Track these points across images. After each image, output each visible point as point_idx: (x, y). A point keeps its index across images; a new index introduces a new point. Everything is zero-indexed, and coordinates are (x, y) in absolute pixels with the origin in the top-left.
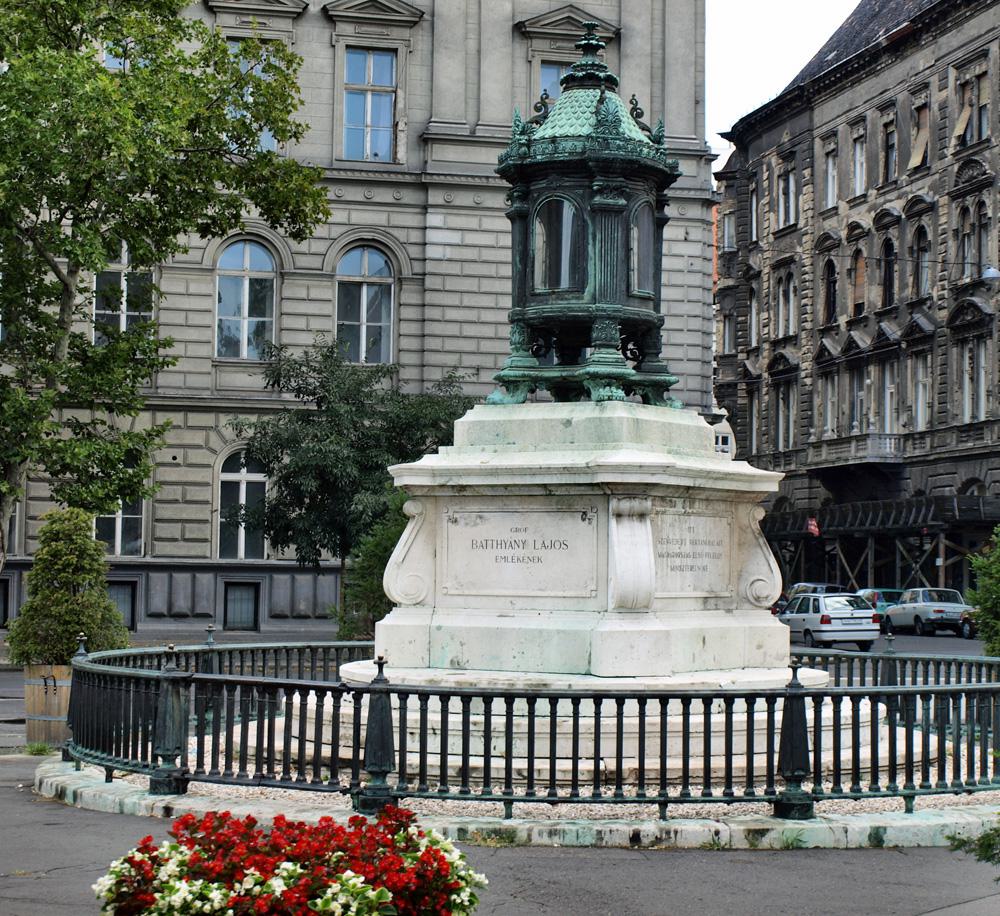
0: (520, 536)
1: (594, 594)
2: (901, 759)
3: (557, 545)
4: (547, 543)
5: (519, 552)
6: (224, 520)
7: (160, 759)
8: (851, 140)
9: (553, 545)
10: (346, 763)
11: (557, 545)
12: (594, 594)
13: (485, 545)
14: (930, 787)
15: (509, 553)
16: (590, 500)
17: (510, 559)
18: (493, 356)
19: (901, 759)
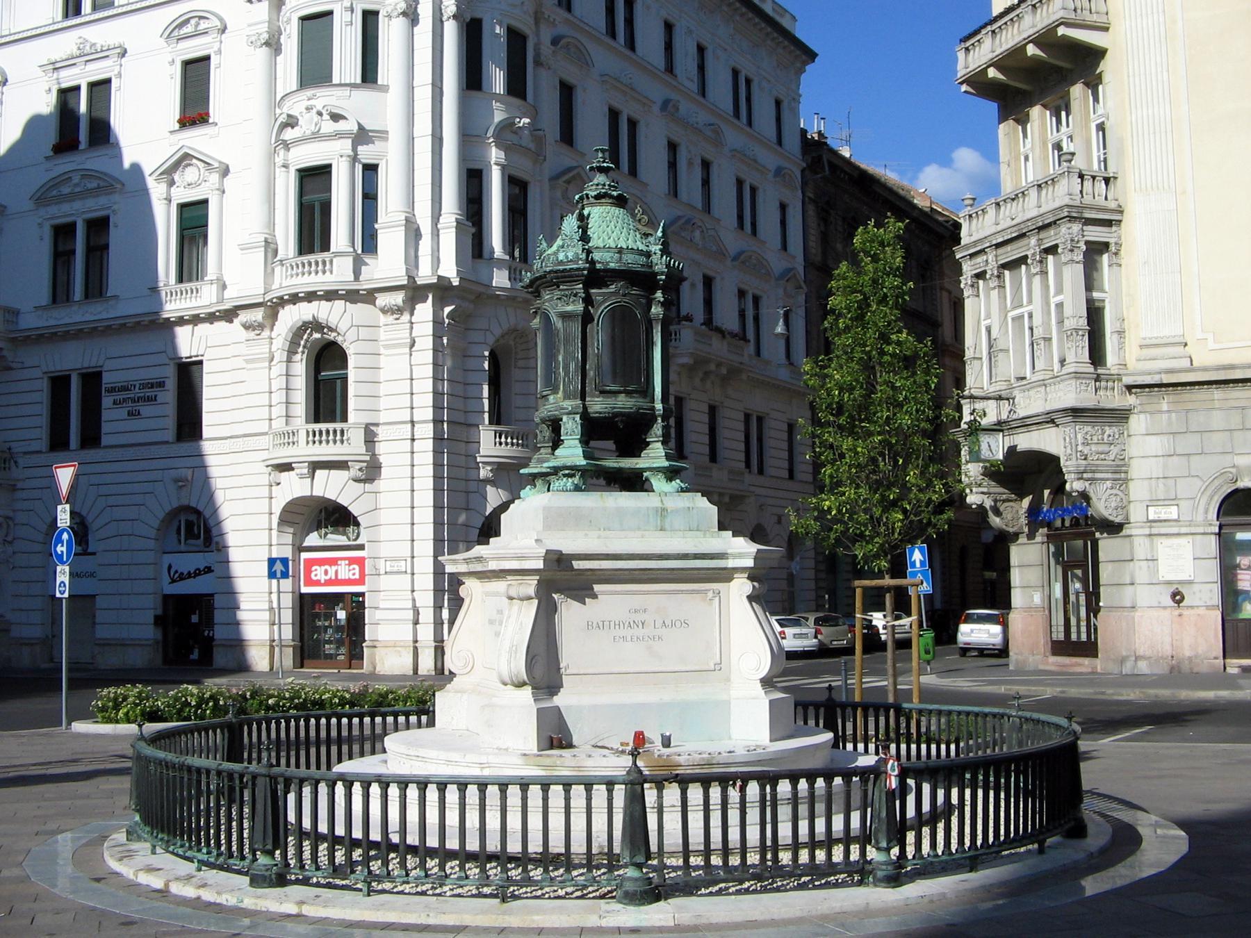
0: (639, 617)
1: (718, 667)
2: (303, 748)
3: (678, 624)
4: (668, 622)
5: (639, 632)
6: (866, 631)
7: (258, 853)
8: (222, 68)
9: (673, 624)
10: (820, 844)
11: (678, 624)
12: (718, 667)
13: (601, 626)
14: (340, 761)
15: (628, 633)
16: (1160, 603)
17: (629, 639)
18: (1199, 434)
19: (303, 748)
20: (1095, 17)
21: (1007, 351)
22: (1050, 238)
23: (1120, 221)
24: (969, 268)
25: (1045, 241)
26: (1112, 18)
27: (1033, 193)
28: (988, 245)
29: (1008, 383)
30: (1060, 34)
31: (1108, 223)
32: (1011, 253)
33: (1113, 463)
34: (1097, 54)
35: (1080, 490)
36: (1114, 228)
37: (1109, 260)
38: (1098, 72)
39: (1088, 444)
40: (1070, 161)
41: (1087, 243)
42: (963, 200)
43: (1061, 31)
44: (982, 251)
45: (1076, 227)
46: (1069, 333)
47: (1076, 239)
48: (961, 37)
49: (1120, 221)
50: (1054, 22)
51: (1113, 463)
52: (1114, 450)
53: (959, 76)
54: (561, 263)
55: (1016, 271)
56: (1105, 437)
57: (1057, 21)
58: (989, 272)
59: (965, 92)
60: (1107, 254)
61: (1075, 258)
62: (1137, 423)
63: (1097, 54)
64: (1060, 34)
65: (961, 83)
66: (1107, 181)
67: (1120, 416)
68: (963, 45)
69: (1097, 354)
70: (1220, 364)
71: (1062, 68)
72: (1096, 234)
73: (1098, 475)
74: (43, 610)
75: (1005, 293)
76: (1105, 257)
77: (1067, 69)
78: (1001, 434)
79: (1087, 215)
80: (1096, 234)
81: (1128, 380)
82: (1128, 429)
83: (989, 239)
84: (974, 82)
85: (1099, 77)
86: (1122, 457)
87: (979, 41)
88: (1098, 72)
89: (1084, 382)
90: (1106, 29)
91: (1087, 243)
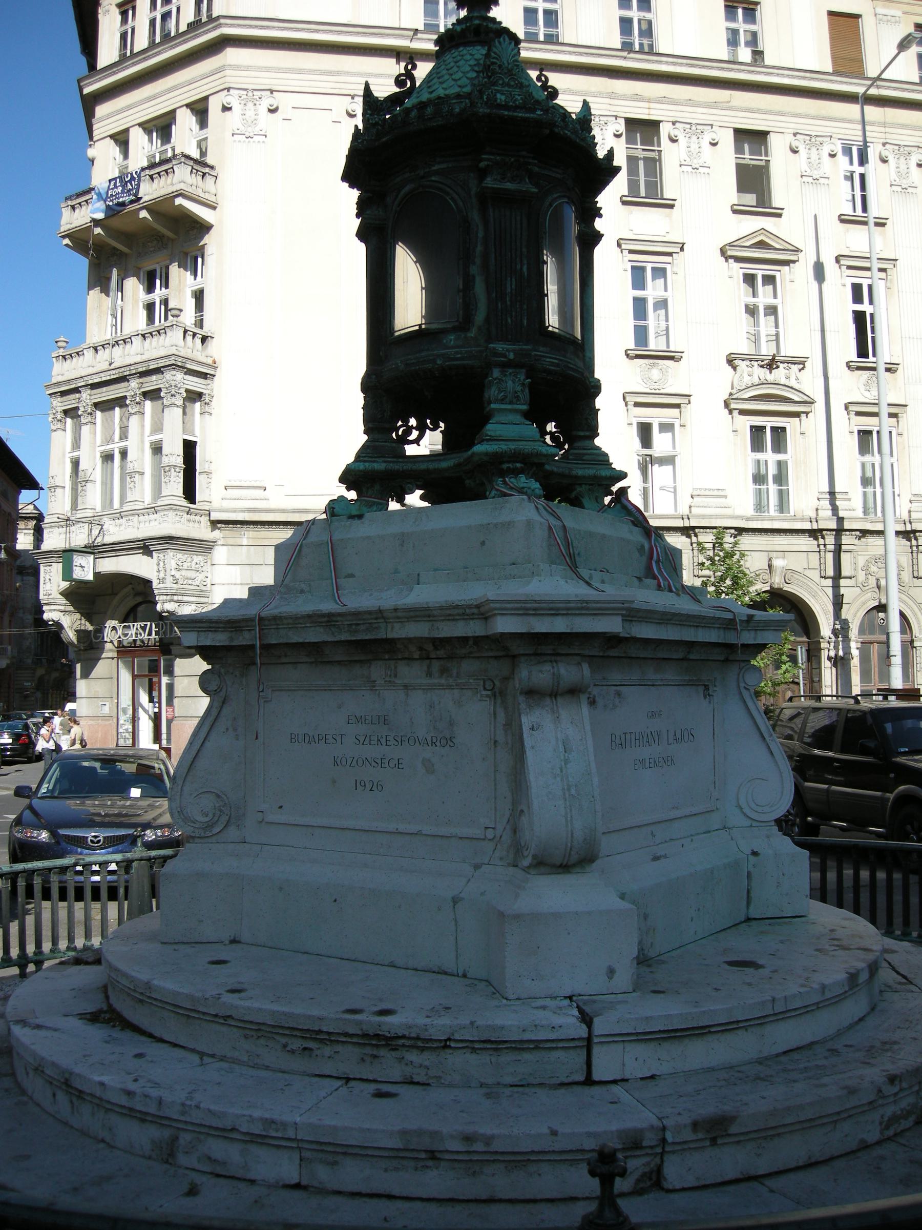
20: (207, 196)
21: (142, 474)
22: (152, 383)
23: (214, 376)
24: (59, 404)
25: (144, 385)
26: (219, 200)
27: (137, 341)
28: (83, 384)
29: (93, 511)
30: (177, 203)
31: (204, 376)
32: (152, 383)
33: (198, 588)
34: (203, 228)
35: (56, 620)
36: (208, 381)
37: (201, 409)
38: (201, 244)
39: (179, 570)
40: (178, 316)
41: (187, 391)
42: (56, 342)
43: (179, 201)
44: (76, 390)
45: (179, 376)
46: (167, 469)
47: (179, 386)
48: (68, 195)
49: (214, 376)
50: (173, 193)
51: (198, 588)
52: (201, 577)
53: (62, 230)
54: (500, 106)
55: (107, 413)
56: (194, 563)
57: (177, 191)
58: (82, 409)
59: (67, 245)
60: (199, 403)
61: (176, 403)
62: (220, 554)
63: (203, 228)
64: (177, 203)
65: (64, 237)
66: (204, 339)
67: (203, 547)
68: (70, 203)
69: (190, 492)
70: (296, 507)
71: (163, 236)
72: (195, 384)
73: (186, 598)
74: (815, 533)
75: (95, 430)
76: (198, 404)
77: (168, 238)
78: (92, 556)
79: (188, 366)
80: (195, 384)
81: (215, 516)
82: (211, 559)
83: (85, 379)
84: (77, 239)
85: (201, 252)
86: (205, 584)
87: (86, 201)
88: (201, 244)
89: (178, 513)
90: (214, 208)
91: (187, 391)
